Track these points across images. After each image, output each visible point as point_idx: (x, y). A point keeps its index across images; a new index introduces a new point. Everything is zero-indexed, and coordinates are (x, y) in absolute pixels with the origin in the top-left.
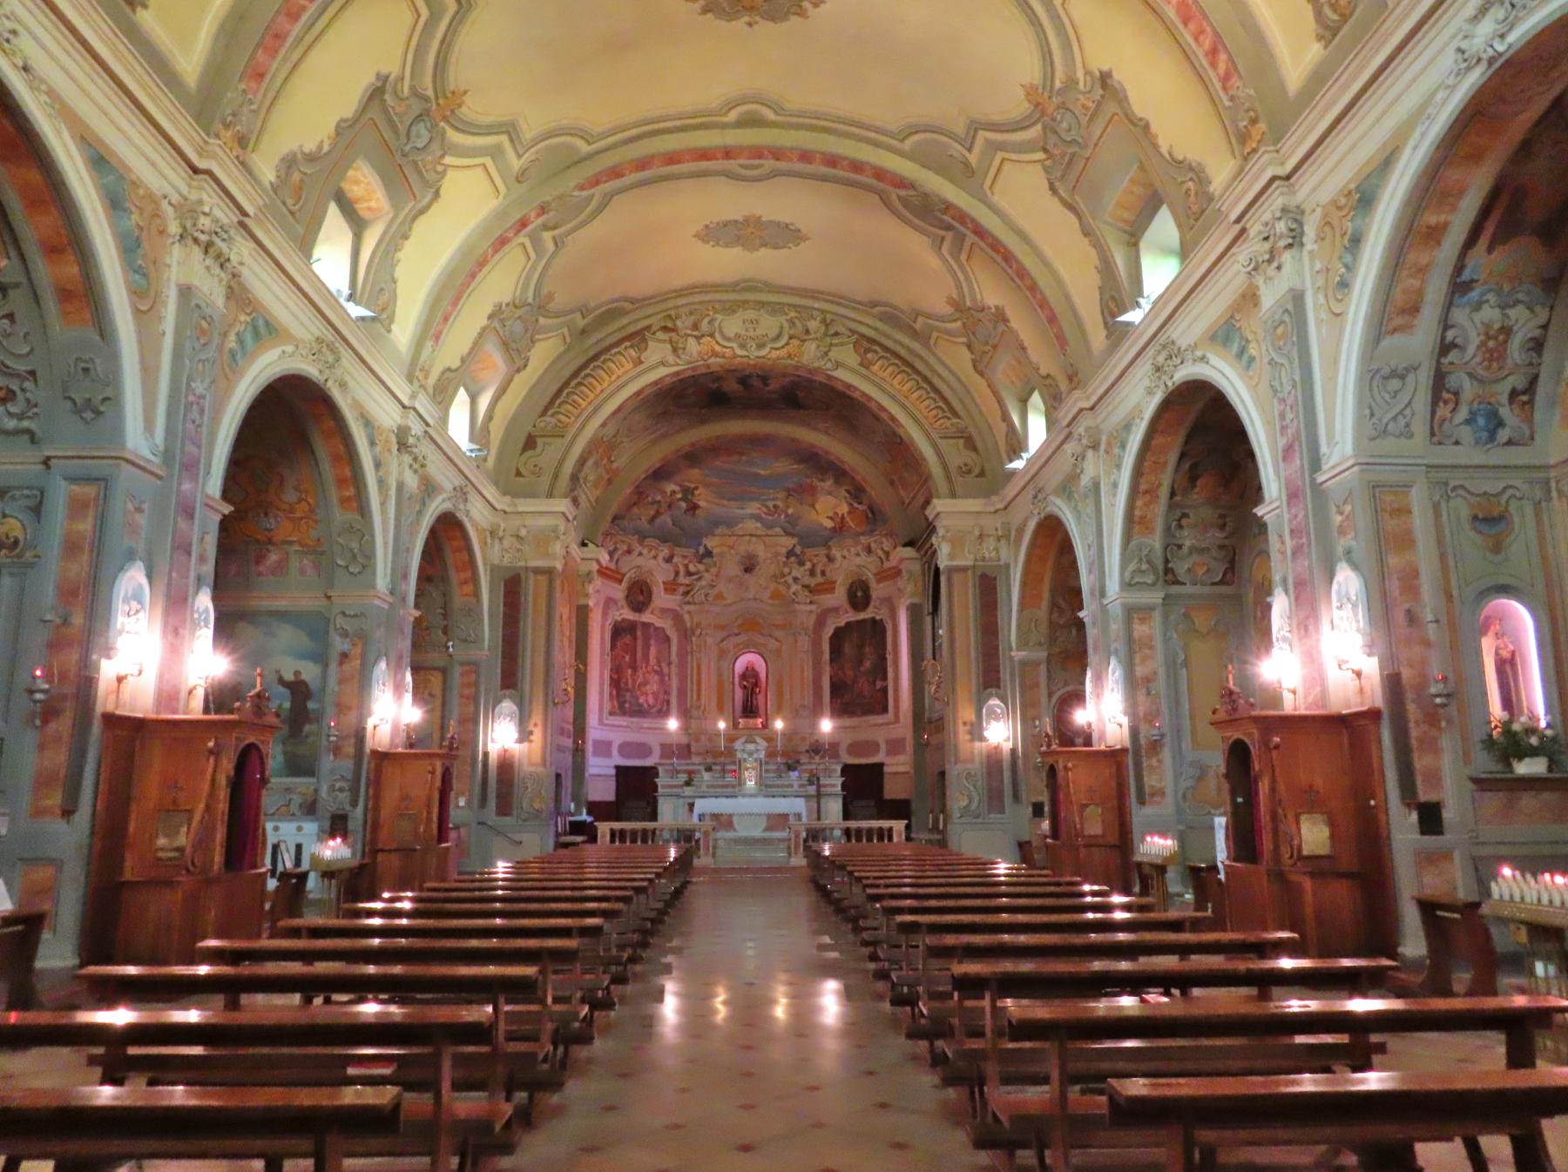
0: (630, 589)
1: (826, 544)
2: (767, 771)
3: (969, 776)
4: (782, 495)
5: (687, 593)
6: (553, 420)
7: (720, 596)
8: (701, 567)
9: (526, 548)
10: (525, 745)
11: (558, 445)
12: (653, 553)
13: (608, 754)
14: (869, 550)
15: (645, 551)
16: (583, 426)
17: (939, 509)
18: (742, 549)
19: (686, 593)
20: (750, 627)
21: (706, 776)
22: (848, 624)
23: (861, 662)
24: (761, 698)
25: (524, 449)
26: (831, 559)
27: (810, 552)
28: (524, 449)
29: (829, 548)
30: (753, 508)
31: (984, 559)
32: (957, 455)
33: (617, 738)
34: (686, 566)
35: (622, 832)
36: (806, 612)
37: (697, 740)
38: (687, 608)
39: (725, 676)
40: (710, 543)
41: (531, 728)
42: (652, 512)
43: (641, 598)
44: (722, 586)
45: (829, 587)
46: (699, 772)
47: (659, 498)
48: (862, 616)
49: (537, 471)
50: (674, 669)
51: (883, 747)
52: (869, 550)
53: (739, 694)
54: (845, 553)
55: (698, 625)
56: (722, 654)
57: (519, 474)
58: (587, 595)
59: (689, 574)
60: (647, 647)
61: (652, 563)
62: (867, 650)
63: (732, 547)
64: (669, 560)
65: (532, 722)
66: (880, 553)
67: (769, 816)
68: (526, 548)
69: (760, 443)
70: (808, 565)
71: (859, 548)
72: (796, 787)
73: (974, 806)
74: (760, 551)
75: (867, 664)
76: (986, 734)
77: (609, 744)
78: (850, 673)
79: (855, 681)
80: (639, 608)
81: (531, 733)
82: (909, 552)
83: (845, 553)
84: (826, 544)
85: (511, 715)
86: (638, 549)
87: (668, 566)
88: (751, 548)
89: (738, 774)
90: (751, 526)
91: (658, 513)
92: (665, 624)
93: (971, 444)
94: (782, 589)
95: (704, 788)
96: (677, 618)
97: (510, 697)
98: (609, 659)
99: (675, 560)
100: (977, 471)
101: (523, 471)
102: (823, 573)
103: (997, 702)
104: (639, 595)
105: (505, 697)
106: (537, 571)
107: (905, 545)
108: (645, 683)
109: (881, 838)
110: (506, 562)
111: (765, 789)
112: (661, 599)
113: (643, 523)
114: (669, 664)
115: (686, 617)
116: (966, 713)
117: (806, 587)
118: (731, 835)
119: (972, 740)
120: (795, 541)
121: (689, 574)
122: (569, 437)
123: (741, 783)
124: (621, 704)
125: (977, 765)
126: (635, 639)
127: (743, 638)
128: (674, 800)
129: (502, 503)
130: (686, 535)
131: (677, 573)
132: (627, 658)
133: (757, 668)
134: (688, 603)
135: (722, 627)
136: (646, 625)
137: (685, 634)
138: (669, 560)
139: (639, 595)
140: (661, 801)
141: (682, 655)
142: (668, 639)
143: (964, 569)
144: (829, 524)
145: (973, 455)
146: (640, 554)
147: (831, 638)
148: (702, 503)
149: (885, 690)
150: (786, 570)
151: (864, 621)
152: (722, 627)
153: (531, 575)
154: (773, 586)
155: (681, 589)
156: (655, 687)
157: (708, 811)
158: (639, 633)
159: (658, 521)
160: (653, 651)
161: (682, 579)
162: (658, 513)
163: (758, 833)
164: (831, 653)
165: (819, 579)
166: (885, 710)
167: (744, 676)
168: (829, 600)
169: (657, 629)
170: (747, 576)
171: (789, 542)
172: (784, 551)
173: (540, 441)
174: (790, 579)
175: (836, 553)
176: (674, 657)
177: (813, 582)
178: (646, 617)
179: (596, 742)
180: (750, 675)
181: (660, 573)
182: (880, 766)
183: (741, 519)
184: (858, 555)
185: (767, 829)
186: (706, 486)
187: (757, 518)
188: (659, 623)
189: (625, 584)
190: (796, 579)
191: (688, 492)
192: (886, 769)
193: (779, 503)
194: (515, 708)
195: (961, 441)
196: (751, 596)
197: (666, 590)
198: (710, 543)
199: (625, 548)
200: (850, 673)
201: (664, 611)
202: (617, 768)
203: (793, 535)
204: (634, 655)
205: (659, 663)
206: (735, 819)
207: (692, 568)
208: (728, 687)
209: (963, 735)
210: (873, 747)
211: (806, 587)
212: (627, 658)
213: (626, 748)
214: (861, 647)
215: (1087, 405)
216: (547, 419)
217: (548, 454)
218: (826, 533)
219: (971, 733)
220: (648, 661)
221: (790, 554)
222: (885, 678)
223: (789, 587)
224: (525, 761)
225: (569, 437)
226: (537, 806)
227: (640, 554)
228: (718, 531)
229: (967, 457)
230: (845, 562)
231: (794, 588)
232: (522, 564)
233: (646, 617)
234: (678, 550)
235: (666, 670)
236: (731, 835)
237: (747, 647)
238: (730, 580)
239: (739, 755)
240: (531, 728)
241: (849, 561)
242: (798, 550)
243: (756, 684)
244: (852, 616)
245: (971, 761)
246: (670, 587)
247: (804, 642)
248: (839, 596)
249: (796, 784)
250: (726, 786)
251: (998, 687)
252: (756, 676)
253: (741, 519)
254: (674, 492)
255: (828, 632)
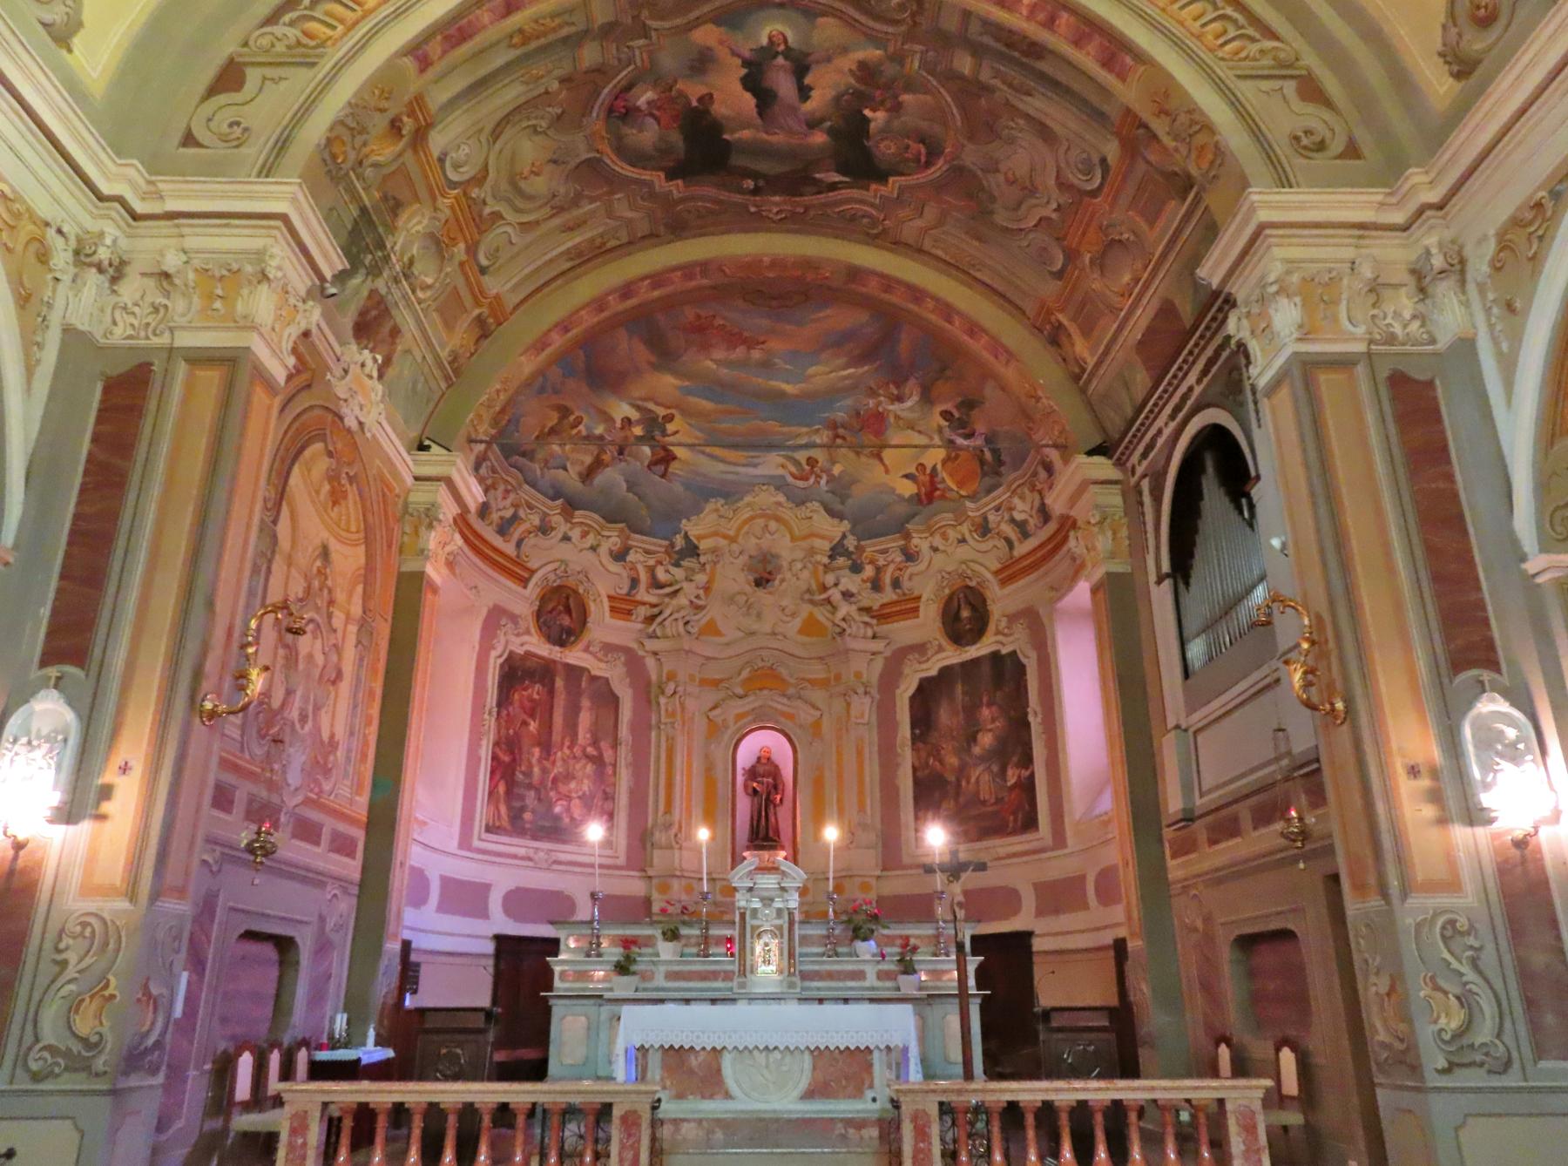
0: (543, 599)
1: (900, 528)
2: (804, 940)
3: (1451, 932)
4: (823, 437)
5: (650, 619)
6: (293, 33)
7: (711, 629)
8: (678, 573)
9: (178, 305)
10: (84, 829)
11: (300, 81)
12: (591, 540)
13: (483, 913)
14: (984, 529)
15: (575, 534)
16: (362, 46)
17: (1264, 216)
18: (751, 544)
19: (650, 619)
20: (764, 684)
21: (666, 950)
22: (946, 672)
23: (972, 739)
24: (783, 814)
25: (212, 91)
26: (910, 556)
27: (871, 547)
28: (212, 91)
29: (908, 536)
30: (772, 464)
31: (1391, 339)
32: (1287, 116)
33: (502, 880)
34: (651, 571)
35: (364, 1115)
36: (865, 656)
37: (664, 888)
38: (651, 645)
39: (721, 773)
40: (694, 528)
41: (110, 776)
42: (588, 460)
43: (566, 621)
44: (714, 611)
45: (908, 607)
46: (649, 941)
47: (599, 430)
48: (973, 652)
49: (238, 135)
50: (624, 753)
51: (1029, 901)
52: (984, 529)
53: (744, 805)
54: (937, 541)
55: (671, 676)
56: (714, 730)
57: (189, 140)
58: (422, 553)
59: (656, 584)
60: (573, 711)
61: (583, 555)
62: (986, 713)
63: (733, 540)
64: (620, 556)
65: (117, 760)
66: (1008, 529)
67: (818, 1054)
68: (178, 305)
69: (784, 293)
70: (869, 571)
71: (965, 529)
72: (871, 980)
73: (1484, 1033)
74: (785, 549)
75: (986, 740)
76: (1486, 799)
77: (483, 889)
78: (952, 760)
79: (962, 771)
80: (563, 638)
81: (106, 792)
82: (1102, 467)
83: (937, 541)
84: (900, 528)
85: (55, 738)
86: (563, 528)
87: (615, 567)
88: (766, 542)
89: (737, 946)
90: (768, 498)
91: (598, 464)
92: (614, 673)
93: (1311, 91)
94: (821, 614)
95: (659, 981)
96: (634, 664)
97: (58, 684)
98: (490, 722)
99: (631, 557)
100: (1337, 146)
101: (200, 133)
102: (896, 584)
103: (1503, 706)
104: (562, 612)
105: (43, 684)
106: (200, 359)
107: (1090, 453)
108: (569, 776)
109: (1186, 1140)
110: (119, 334)
111: (805, 983)
112: (604, 626)
113: (570, 479)
114: (615, 745)
115: (650, 662)
116: (1408, 738)
117: (866, 610)
118: (713, 1107)
119: (1443, 821)
120: (846, 525)
121: (656, 584)
122: (326, 66)
123: (745, 970)
124: (516, 816)
125: (1468, 899)
126: (551, 692)
127: (751, 703)
128: (589, 1007)
129: (119, 177)
130: (651, 519)
131: (634, 582)
132: (533, 726)
133: (775, 757)
134: (653, 636)
135: (716, 683)
136: (574, 672)
137: (646, 694)
138: (620, 556)
139: (562, 612)
140: (558, 1009)
141: (641, 728)
142: (615, 700)
143: (1343, 363)
144: (908, 489)
145: (1327, 115)
146: (566, 538)
147: (913, 699)
148: (679, 452)
149: (1028, 787)
150: (830, 579)
151: (976, 662)
152: (716, 683)
153: (182, 369)
154: (806, 609)
155: (643, 611)
156: (586, 786)
157: (655, 1040)
158: (559, 683)
159: (600, 479)
160: (585, 719)
161: (642, 594)
162: (598, 464)
163: (786, 1101)
164: (913, 726)
165: (889, 595)
166: (1030, 823)
167: (752, 773)
168: (904, 632)
169: (594, 679)
170: (760, 592)
171: (836, 529)
172: (827, 546)
173: (253, 76)
174: (835, 594)
175: (920, 542)
176: (624, 732)
177: (876, 601)
178: (574, 656)
179: (351, 854)
180: (764, 770)
181: (604, 585)
182: (1024, 938)
183: (750, 486)
184: (963, 541)
185: (809, 1095)
186: (687, 412)
187: (780, 485)
188: (597, 668)
189: (533, 590)
190: (847, 595)
191: (655, 426)
192: (1038, 944)
193: (818, 454)
194: (69, 716)
195: (1290, 87)
196: (767, 628)
197: (613, 610)
198: (694, 528)
199: (536, 520)
200: (952, 760)
201: (609, 648)
202: (499, 939)
203: (839, 516)
204: (548, 726)
205: (595, 743)
206: (727, 1063)
207: (661, 575)
208: (723, 789)
209: (1412, 808)
210: (1008, 900)
211: (866, 610)
212: (533, 726)
213: (517, 902)
214: (971, 711)
215: (1433, 197)
216: (278, 30)
217: (265, 104)
218: (901, 509)
219: (1435, 796)
220: (574, 735)
221: (837, 550)
222: (1027, 760)
223: (835, 608)
224: (76, 877)
225: (326, 66)
226: (84, 1025)
227: (566, 538)
228: (710, 506)
229: (1312, 117)
230: (938, 558)
231: (844, 609)
232: (164, 340)
233: (574, 656)
234: (637, 540)
235: (608, 755)
236: (713, 1107)
237: (761, 719)
238: (731, 600)
239: (741, 901)
240: (110, 776)
241: (945, 555)
242: (851, 543)
243: (776, 786)
244: (953, 656)
245: (1452, 885)
246: (622, 607)
247: (864, 708)
248: (927, 624)
249: (871, 972)
250: (714, 975)
251: (1494, 665)
252: (775, 773)
253: (750, 486)
254: (627, 422)
255: (907, 689)
